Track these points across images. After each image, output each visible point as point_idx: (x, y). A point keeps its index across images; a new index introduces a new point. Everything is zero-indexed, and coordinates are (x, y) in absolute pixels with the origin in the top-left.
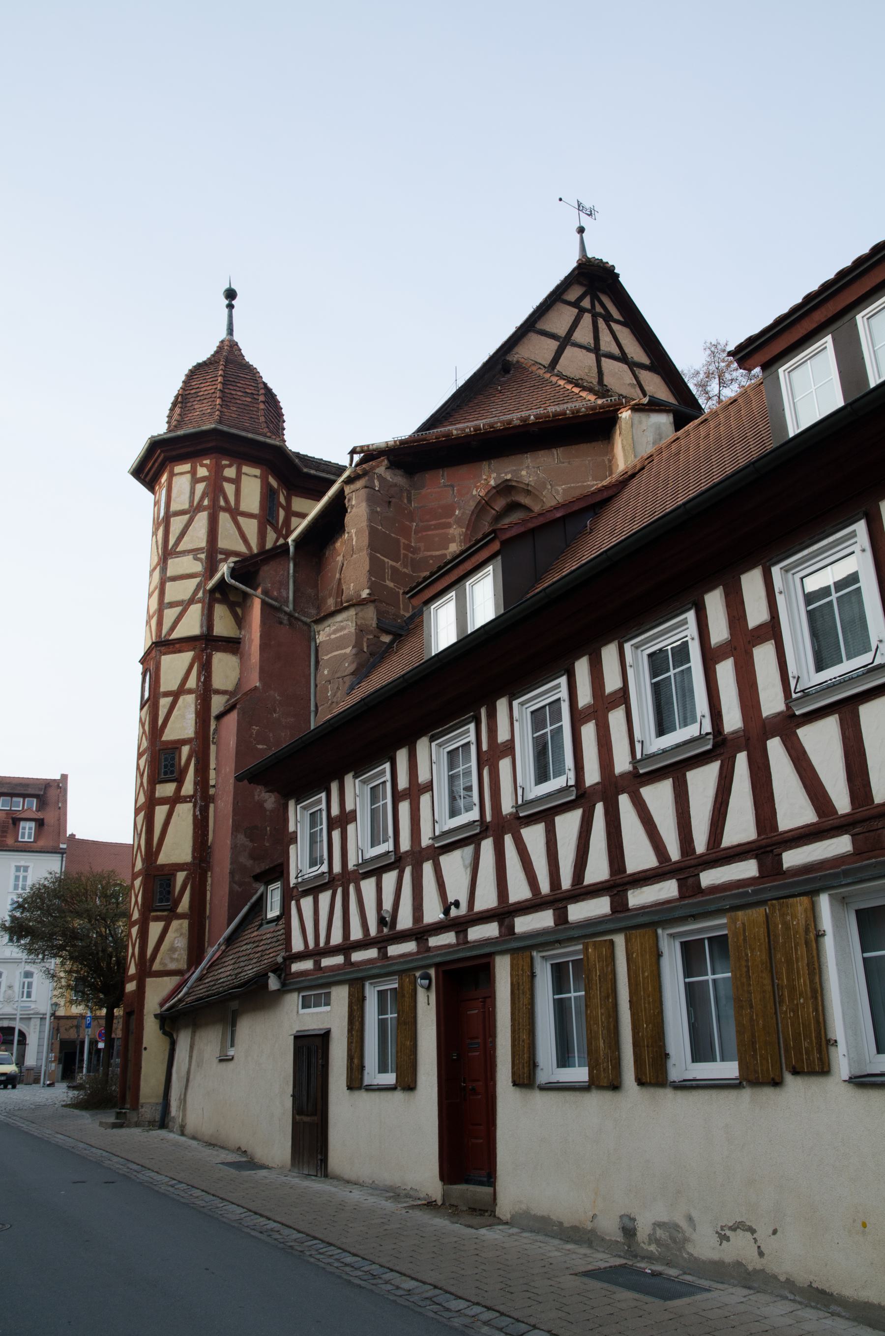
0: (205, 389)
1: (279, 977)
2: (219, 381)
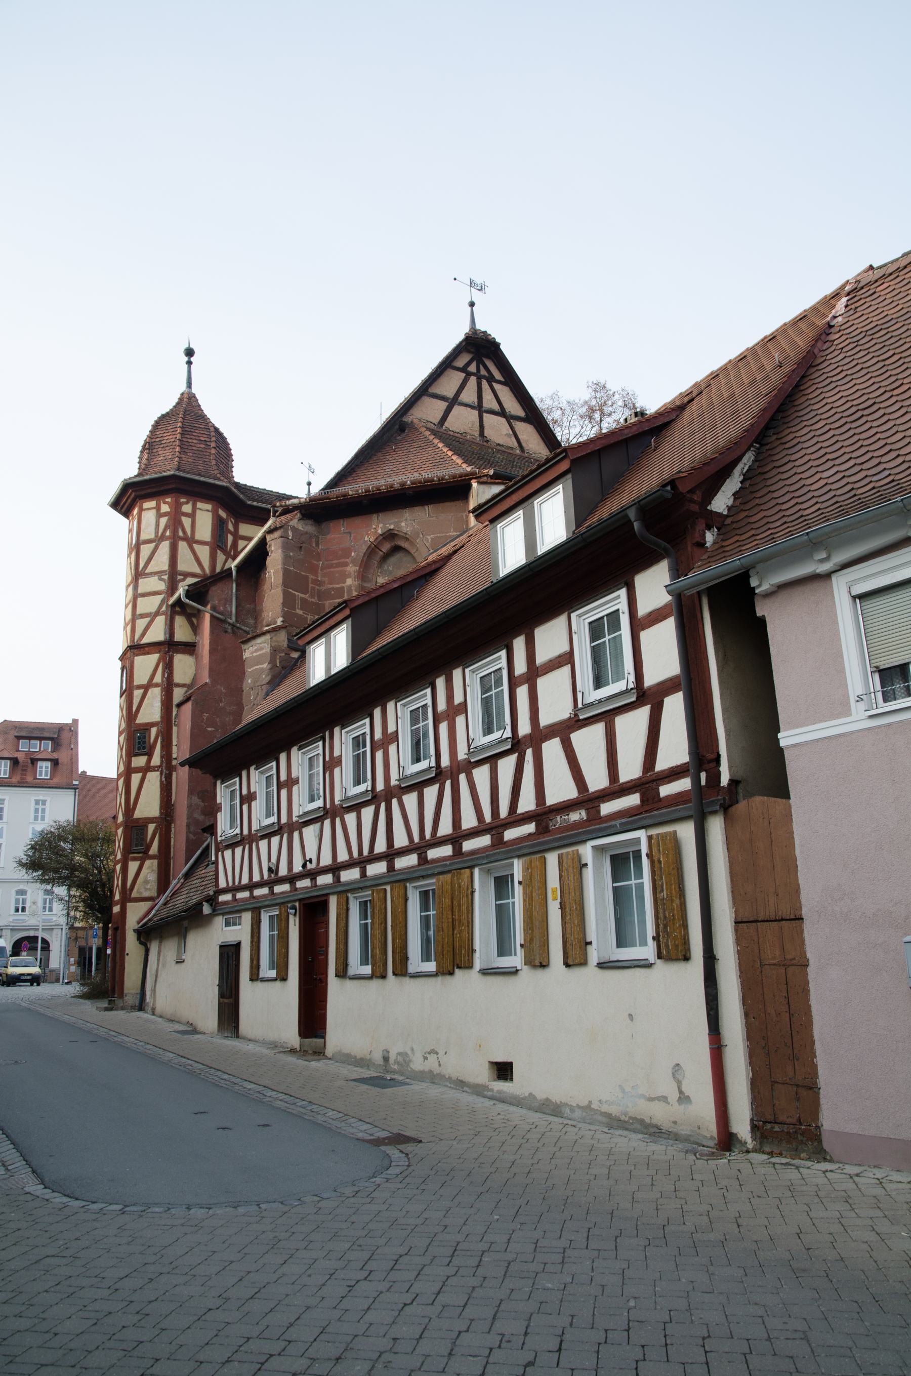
0: (167, 438)
1: (211, 905)
2: (178, 432)
